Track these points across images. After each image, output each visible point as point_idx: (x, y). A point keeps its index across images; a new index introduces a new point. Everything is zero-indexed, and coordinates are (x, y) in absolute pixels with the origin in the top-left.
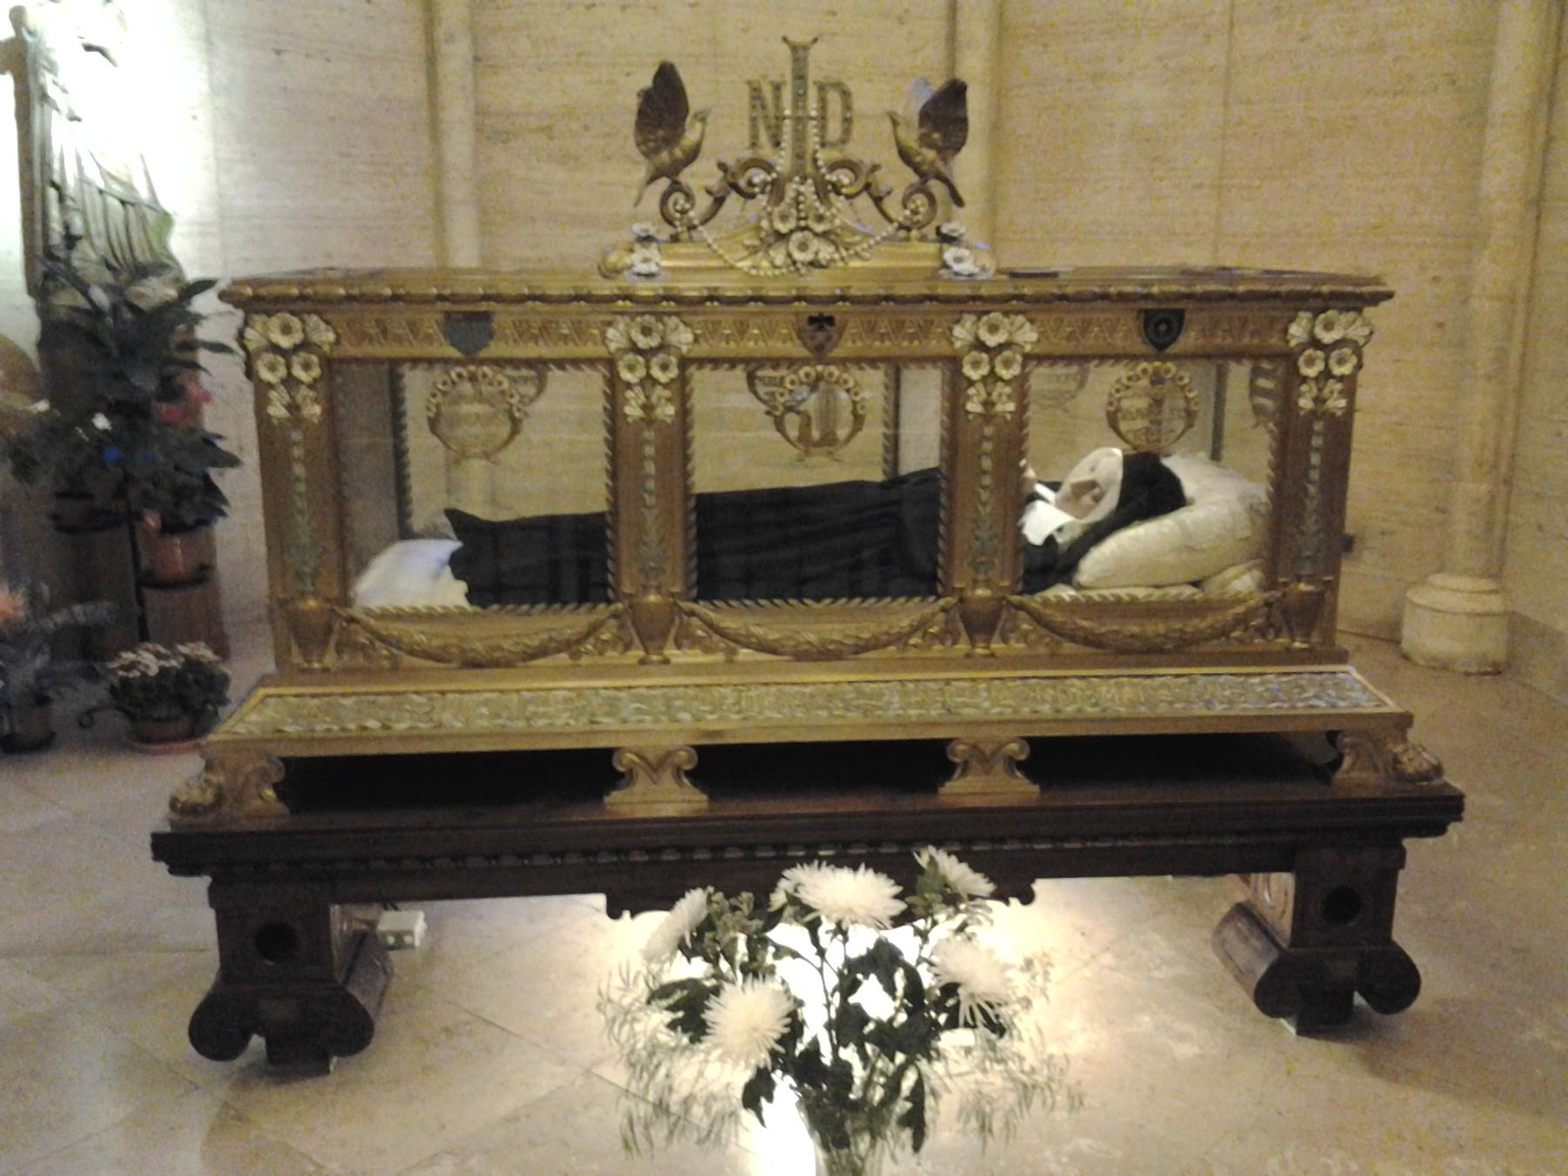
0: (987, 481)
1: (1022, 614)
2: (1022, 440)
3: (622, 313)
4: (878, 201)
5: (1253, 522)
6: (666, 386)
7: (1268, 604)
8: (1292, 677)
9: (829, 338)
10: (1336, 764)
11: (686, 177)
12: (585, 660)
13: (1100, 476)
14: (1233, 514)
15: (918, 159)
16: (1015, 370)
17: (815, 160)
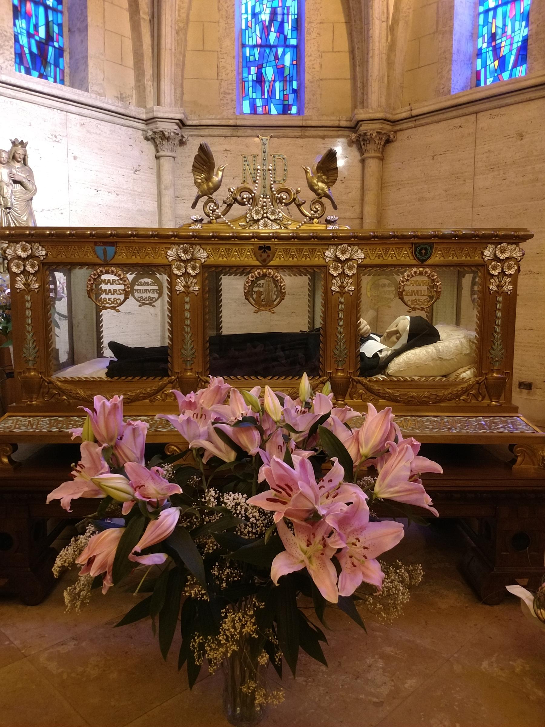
0: (342, 323)
1: (359, 385)
2: (358, 305)
3: (174, 244)
4: (299, 206)
5: (470, 346)
6: (194, 277)
7: (478, 383)
8: (492, 418)
9: (268, 256)
10: (514, 461)
11: (214, 196)
12: (156, 403)
13: (400, 327)
14: (461, 343)
15: (316, 187)
16: (355, 271)
17: (271, 188)
